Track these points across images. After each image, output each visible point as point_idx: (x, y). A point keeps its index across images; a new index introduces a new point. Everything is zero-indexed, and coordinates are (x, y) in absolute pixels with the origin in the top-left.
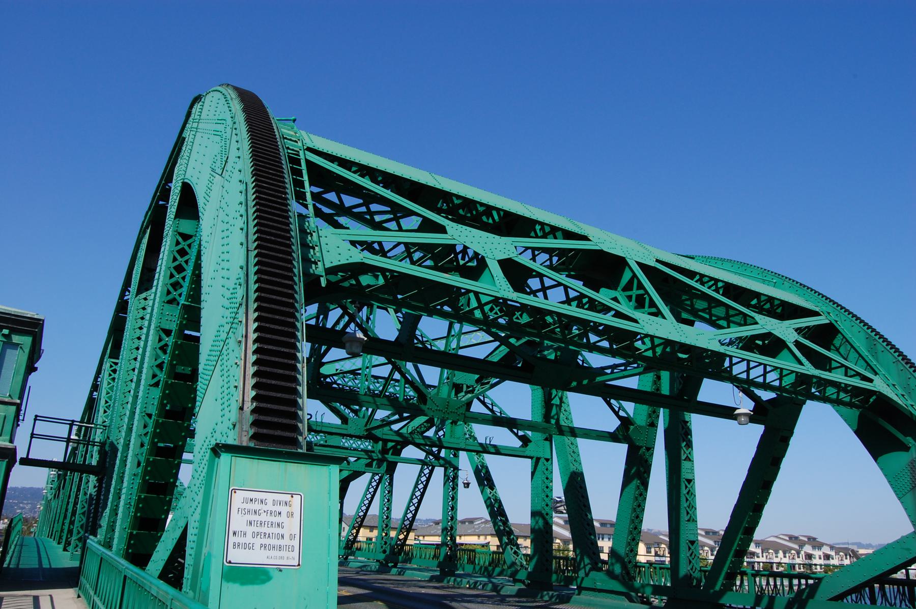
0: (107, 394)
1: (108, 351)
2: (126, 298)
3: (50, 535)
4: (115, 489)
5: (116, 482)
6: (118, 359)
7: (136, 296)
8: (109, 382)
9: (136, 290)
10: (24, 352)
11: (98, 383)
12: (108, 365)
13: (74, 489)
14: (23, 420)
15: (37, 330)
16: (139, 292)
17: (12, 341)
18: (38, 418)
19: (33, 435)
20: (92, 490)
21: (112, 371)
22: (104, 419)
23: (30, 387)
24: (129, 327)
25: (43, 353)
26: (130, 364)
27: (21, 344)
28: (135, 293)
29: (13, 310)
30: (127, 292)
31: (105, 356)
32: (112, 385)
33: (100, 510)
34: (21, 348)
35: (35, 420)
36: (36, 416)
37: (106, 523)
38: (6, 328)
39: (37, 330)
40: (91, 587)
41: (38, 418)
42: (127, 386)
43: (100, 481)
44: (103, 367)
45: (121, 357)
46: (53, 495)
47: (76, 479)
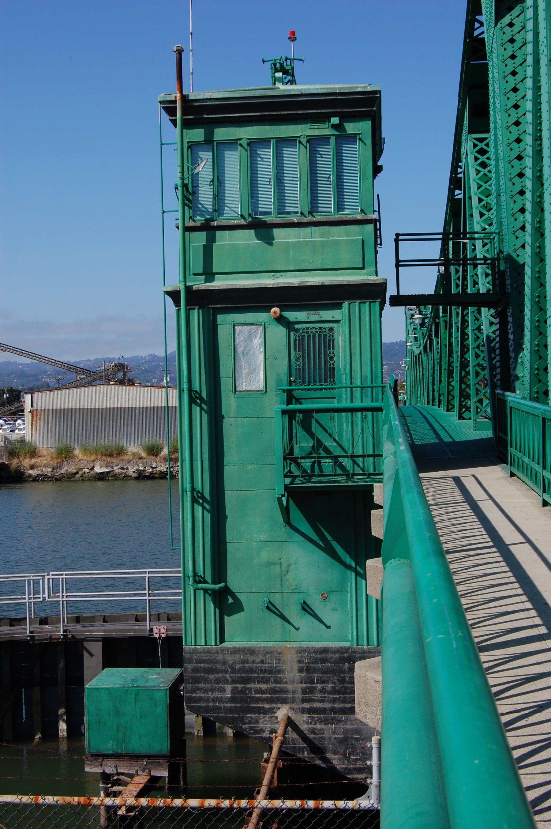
0: (478, 189)
1: (466, 123)
2: (476, 33)
3: (431, 401)
4: (531, 321)
5: (531, 311)
6: (488, 131)
7: (496, 24)
8: (476, 170)
9: (493, 15)
10: (365, 145)
11: (459, 176)
12: (470, 144)
13: (457, 335)
14: (381, 244)
15: (375, 109)
16: (499, 16)
17: (346, 131)
18: (400, 238)
19: (398, 264)
20: (487, 330)
21: (477, 152)
22: (483, 225)
23: (378, 196)
24: (496, 75)
25: (384, 143)
26: (510, 132)
27: (359, 134)
28: (493, 18)
29: (337, 86)
30: (476, 23)
31: (462, 132)
32: (482, 173)
33: (512, 355)
34: (360, 139)
35: (397, 241)
36: (397, 235)
37: (529, 371)
38: (334, 115)
39: (375, 109)
40: (533, 461)
41: (400, 238)
42: (513, 167)
43: (501, 316)
44: (462, 150)
45: (492, 125)
46: (422, 347)
47: (456, 320)
